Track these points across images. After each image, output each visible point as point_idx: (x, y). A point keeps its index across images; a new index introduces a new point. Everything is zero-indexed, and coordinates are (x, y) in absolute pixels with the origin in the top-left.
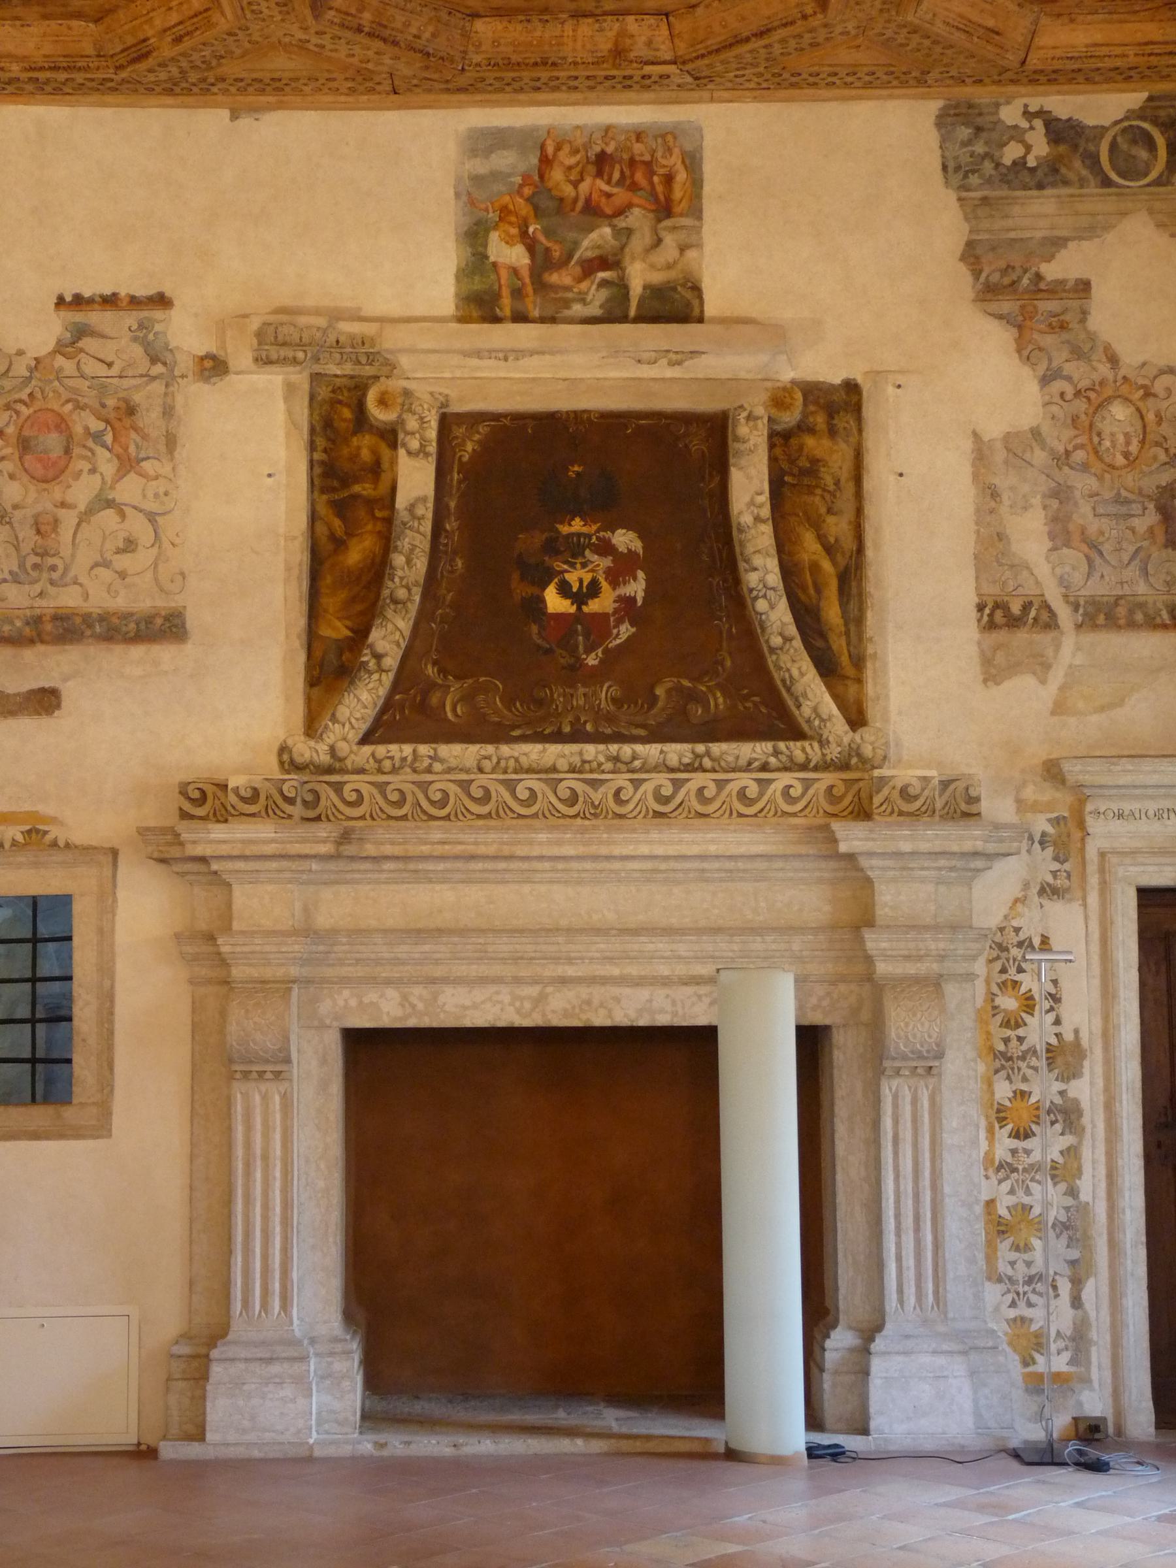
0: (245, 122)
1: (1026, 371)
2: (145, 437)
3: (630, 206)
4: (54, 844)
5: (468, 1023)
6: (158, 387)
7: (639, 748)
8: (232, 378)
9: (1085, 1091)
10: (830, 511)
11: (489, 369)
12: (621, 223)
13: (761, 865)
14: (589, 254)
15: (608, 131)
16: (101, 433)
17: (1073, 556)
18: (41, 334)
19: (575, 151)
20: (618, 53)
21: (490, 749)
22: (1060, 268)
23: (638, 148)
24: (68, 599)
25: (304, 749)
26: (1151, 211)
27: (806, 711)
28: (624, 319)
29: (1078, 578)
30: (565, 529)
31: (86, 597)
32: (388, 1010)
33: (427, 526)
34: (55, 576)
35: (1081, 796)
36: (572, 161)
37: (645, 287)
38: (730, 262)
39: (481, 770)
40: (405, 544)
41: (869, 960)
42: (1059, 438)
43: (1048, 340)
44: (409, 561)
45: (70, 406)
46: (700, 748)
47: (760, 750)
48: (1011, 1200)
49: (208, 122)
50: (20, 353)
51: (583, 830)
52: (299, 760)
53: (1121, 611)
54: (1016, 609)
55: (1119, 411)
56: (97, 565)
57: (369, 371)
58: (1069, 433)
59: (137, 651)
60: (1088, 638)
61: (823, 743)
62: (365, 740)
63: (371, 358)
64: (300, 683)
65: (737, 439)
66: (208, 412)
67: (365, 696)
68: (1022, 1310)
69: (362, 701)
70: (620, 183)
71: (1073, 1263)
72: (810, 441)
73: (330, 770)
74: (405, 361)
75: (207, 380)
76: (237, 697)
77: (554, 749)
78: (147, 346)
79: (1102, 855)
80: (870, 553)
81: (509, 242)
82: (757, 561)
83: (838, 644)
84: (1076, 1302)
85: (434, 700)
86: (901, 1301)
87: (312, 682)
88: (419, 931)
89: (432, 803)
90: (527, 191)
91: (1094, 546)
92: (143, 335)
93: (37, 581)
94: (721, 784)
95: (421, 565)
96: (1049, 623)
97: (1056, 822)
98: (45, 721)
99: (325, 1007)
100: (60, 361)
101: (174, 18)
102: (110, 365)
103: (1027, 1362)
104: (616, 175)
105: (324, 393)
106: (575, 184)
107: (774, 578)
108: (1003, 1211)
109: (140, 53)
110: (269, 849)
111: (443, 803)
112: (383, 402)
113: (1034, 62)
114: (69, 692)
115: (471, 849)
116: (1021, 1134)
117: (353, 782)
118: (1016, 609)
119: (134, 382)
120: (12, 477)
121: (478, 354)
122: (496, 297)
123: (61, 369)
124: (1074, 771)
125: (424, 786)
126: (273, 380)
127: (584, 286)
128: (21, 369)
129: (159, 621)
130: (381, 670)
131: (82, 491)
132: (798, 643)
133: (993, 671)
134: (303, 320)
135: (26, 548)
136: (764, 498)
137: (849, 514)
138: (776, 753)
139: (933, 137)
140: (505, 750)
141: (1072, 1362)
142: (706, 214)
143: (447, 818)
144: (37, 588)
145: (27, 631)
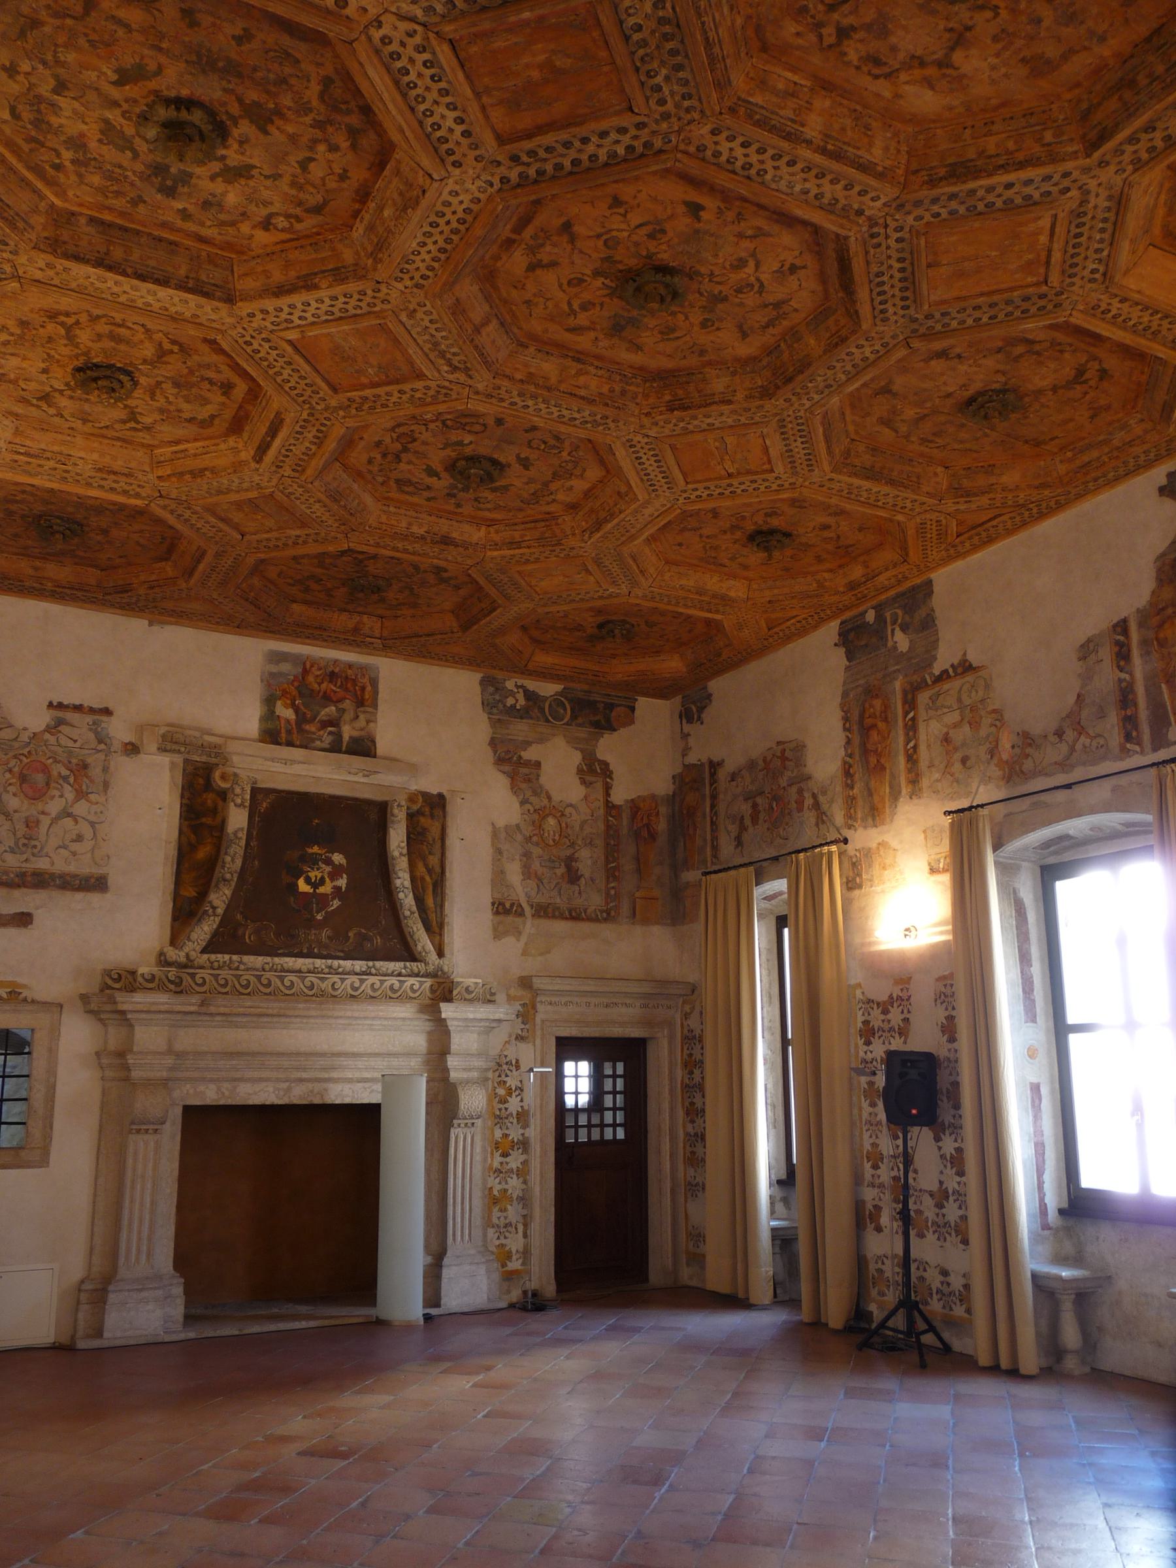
0: (155, 628)
1: (514, 798)
2: (92, 781)
3: (345, 698)
4: (25, 1000)
5: (251, 1102)
6: (101, 756)
7: (341, 962)
8: (142, 756)
9: (532, 1132)
10: (430, 853)
11: (278, 767)
12: (340, 706)
13: (400, 1023)
14: (325, 718)
15: (336, 661)
16: (68, 777)
17: (532, 883)
18: (35, 719)
19: (320, 669)
20: (356, 630)
21: (269, 959)
22: (529, 754)
23: (349, 672)
24: (42, 864)
25: (172, 954)
26: (565, 736)
27: (419, 948)
28: (340, 751)
29: (533, 893)
30: (310, 851)
31: (53, 864)
32: (210, 1095)
33: (243, 843)
34: (35, 851)
35: (536, 993)
36: (319, 673)
37: (350, 737)
38: (388, 732)
39: (264, 970)
40: (231, 851)
41: (446, 1070)
42: (528, 830)
43: (524, 786)
44: (233, 860)
45: (51, 761)
46: (370, 963)
47: (397, 966)
48: (499, 1187)
49: (136, 626)
50: (25, 729)
51: (321, 1003)
52: (169, 960)
53: (550, 910)
54: (508, 905)
55: (551, 821)
56: (60, 847)
57: (214, 760)
58: (531, 828)
59: (79, 896)
60: (537, 921)
61: (426, 964)
62: (203, 951)
63: (217, 755)
64: (169, 918)
65: (393, 815)
66: (126, 770)
67: (206, 928)
68: (503, 1241)
69: (203, 931)
70: (340, 687)
71: (524, 1216)
72: (422, 820)
73: (185, 966)
74: (235, 759)
75: (128, 755)
76: (134, 922)
77: (300, 961)
78: (96, 733)
79: (543, 1021)
80: (447, 874)
81: (286, 707)
82: (401, 874)
83: (432, 916)
84: (525, 1236)
85: (240, 932)
86: (454, 1240)
87: (175, 919)
88: (232, 1053)
89: (242, 986)
90: (296, 684)
91: (540, 880)
92: (95, 728)
93: (24, 853)
94: (382, 982)
95: (239, 862)
96: (521, 913)
97: (523, 1005)
98: (23, 930)
99: (176, 1094)
100: (47, 736)
101: (154, 577)
102: (75, 741)
103: (504, 1265)
104: (339, 683)
105: (190, 768)
106: (319, 684)
107: (407, 883)
108: (496, 1193)
109: (125, 589)
110: (163, 1008)
111: (247, 987)
112: (223, 777)
113: (530, 666)
114: (39, 915)
115: (264, 1011)
116: (505, 1155)
117: (202, 974)
118: (508, 905)
119: (87, 752)
120: (14, 795)
121: (273, 760)
122: (279, 732)
123: (47, 740)
124: (537, 983)
125: (238, 977)
126: (165, 760)
127: (321, 733)
128: (25, 737)
129: (93, 880)
130: (215, 915)
131: (54, 807)
132: (416, 915)
133: (498, 935)
134: (188, 732)
135: (19, 834)
136: (404, 844)
137: (438, 855)
138: (405, 968)
139: (478, 689)
140: (276, 960)
141: (523, 1264)
142: (380, 708)
143: (249, 994)
144: (25, 856)
145: (16, 880)
